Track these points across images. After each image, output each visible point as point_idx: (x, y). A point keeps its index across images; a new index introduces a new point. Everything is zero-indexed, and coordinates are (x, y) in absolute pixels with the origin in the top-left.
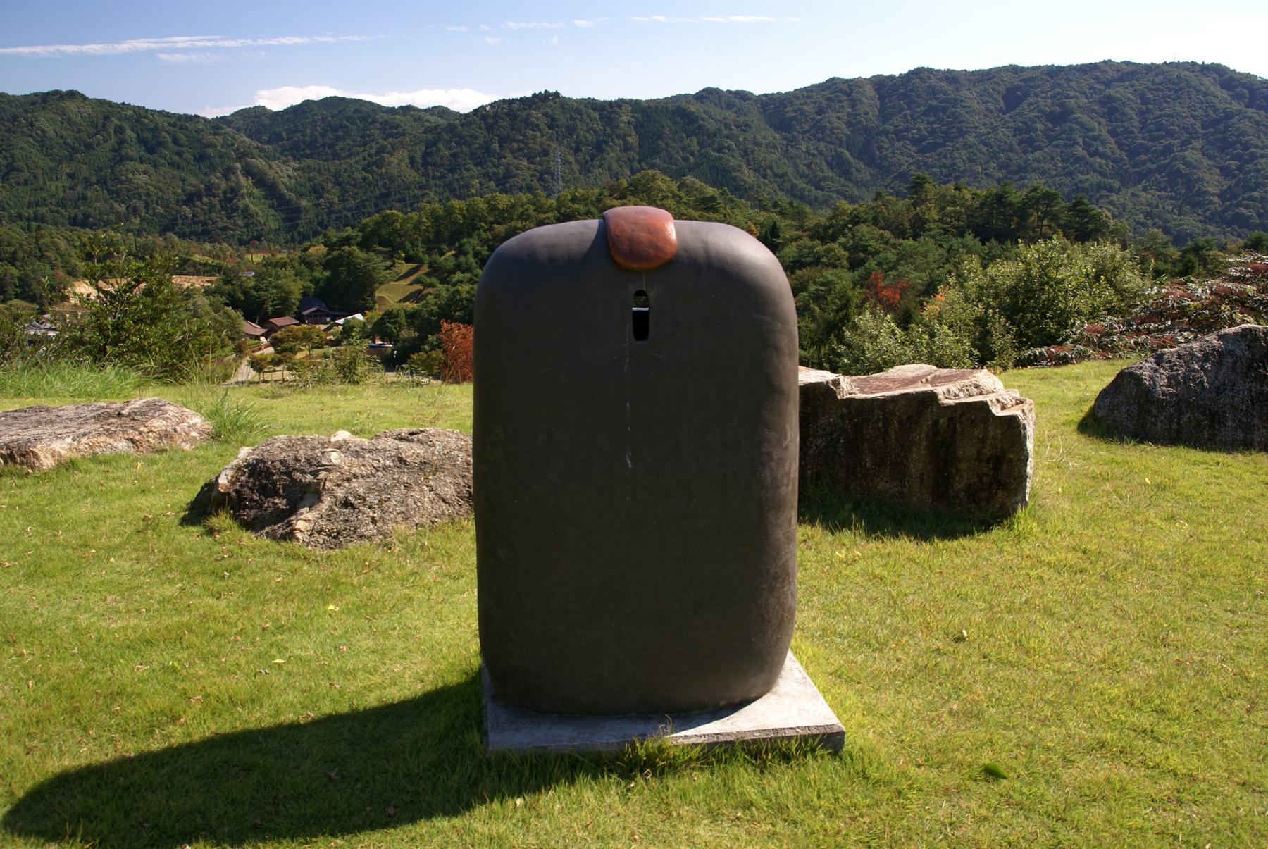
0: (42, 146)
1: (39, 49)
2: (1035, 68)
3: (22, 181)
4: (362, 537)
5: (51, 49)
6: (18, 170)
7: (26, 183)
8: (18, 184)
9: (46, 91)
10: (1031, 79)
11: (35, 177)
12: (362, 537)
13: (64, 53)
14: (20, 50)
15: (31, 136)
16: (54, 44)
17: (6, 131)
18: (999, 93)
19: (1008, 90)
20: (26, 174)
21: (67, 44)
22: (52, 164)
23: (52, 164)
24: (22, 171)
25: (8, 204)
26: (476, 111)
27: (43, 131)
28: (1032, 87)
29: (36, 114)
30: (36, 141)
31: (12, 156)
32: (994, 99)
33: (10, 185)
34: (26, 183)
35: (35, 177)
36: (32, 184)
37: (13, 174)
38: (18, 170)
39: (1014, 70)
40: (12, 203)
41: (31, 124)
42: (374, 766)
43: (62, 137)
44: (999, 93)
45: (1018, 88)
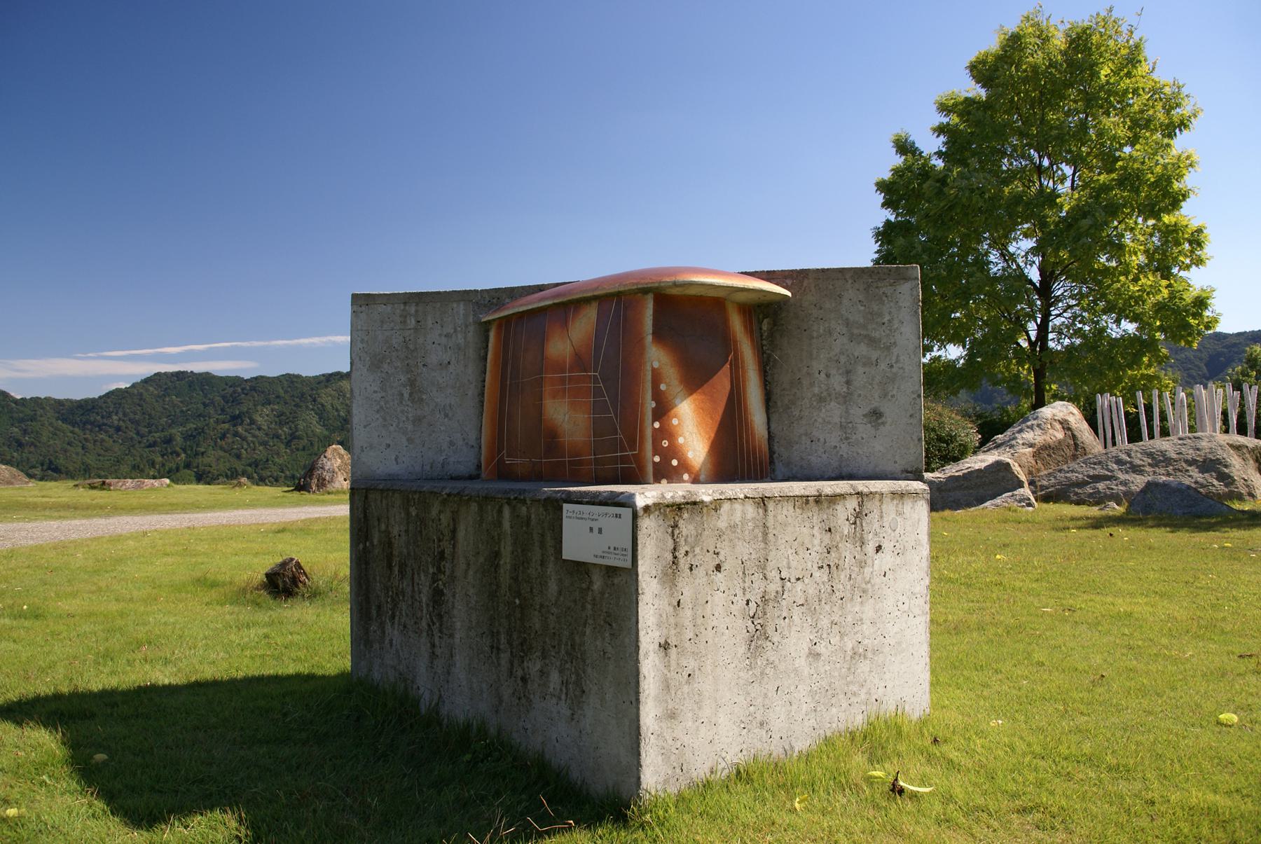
0: (320, 418)
1: (316, 340)
2: (1239, 334)
3: (301, 447)
4: (1031, 446)
5: (324, 339)
6: (299, 438)
7: (304, 449)
8: (298, 450)
9: (330, 372)
10: (1235, 345)
11: (311, 444)
12: (1031, 446)
13: (334, 343)
14: (274, 343)
15: (312, 409)
16: (326, 335)
17: (295, 406)
18: (1201, 359)
19: (1210, 356)
20: (305, 442)
21: (336, 335)
22: (326, 433)
23: (326, 433)
24: (302, 439)
25: (286, 466)
26: (31, 399)
27: (323, 405)
28: (1236, 353)
29: (319, 391)
30: (316, 414)
31: (296, 426)
32: (1196, 366)
33: (292, 450)
34: (304, 449)
35: (311, 444)
36: (309, 450)
37: (295, 441)
38: (299, 438)
39: (1253, 331)
40: (289, 466)
41: (314, 400)
42: (822, 839)
43: (337, 410)
44: (1201, 359)
45: (1219, 354)
